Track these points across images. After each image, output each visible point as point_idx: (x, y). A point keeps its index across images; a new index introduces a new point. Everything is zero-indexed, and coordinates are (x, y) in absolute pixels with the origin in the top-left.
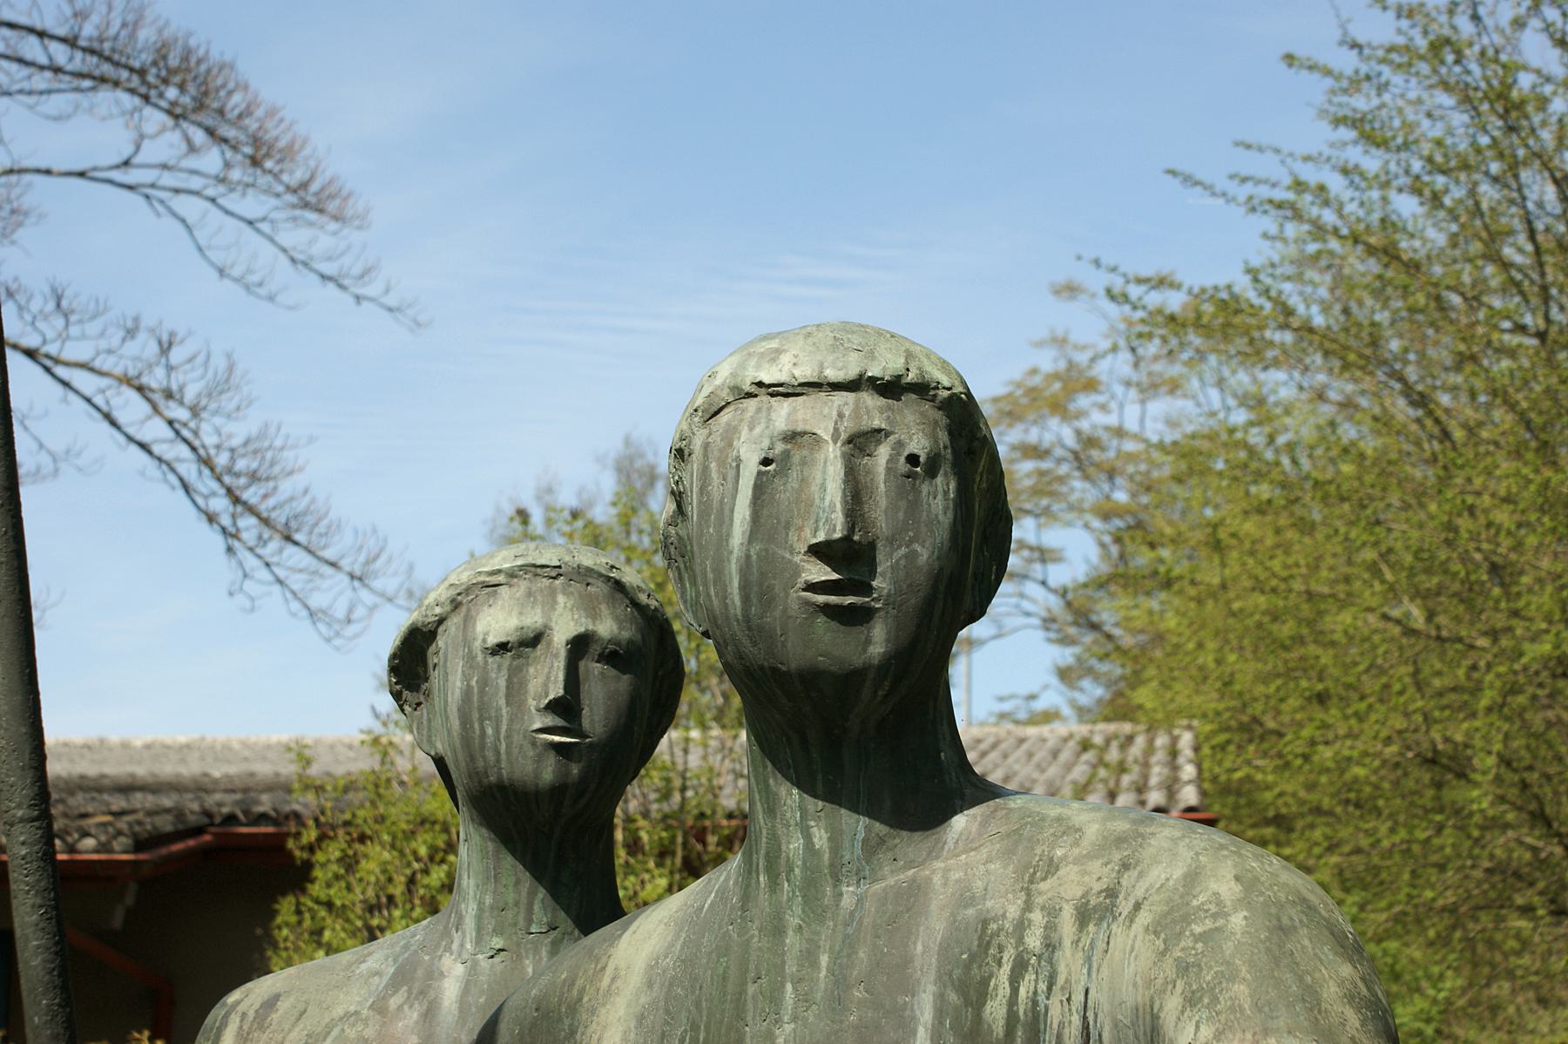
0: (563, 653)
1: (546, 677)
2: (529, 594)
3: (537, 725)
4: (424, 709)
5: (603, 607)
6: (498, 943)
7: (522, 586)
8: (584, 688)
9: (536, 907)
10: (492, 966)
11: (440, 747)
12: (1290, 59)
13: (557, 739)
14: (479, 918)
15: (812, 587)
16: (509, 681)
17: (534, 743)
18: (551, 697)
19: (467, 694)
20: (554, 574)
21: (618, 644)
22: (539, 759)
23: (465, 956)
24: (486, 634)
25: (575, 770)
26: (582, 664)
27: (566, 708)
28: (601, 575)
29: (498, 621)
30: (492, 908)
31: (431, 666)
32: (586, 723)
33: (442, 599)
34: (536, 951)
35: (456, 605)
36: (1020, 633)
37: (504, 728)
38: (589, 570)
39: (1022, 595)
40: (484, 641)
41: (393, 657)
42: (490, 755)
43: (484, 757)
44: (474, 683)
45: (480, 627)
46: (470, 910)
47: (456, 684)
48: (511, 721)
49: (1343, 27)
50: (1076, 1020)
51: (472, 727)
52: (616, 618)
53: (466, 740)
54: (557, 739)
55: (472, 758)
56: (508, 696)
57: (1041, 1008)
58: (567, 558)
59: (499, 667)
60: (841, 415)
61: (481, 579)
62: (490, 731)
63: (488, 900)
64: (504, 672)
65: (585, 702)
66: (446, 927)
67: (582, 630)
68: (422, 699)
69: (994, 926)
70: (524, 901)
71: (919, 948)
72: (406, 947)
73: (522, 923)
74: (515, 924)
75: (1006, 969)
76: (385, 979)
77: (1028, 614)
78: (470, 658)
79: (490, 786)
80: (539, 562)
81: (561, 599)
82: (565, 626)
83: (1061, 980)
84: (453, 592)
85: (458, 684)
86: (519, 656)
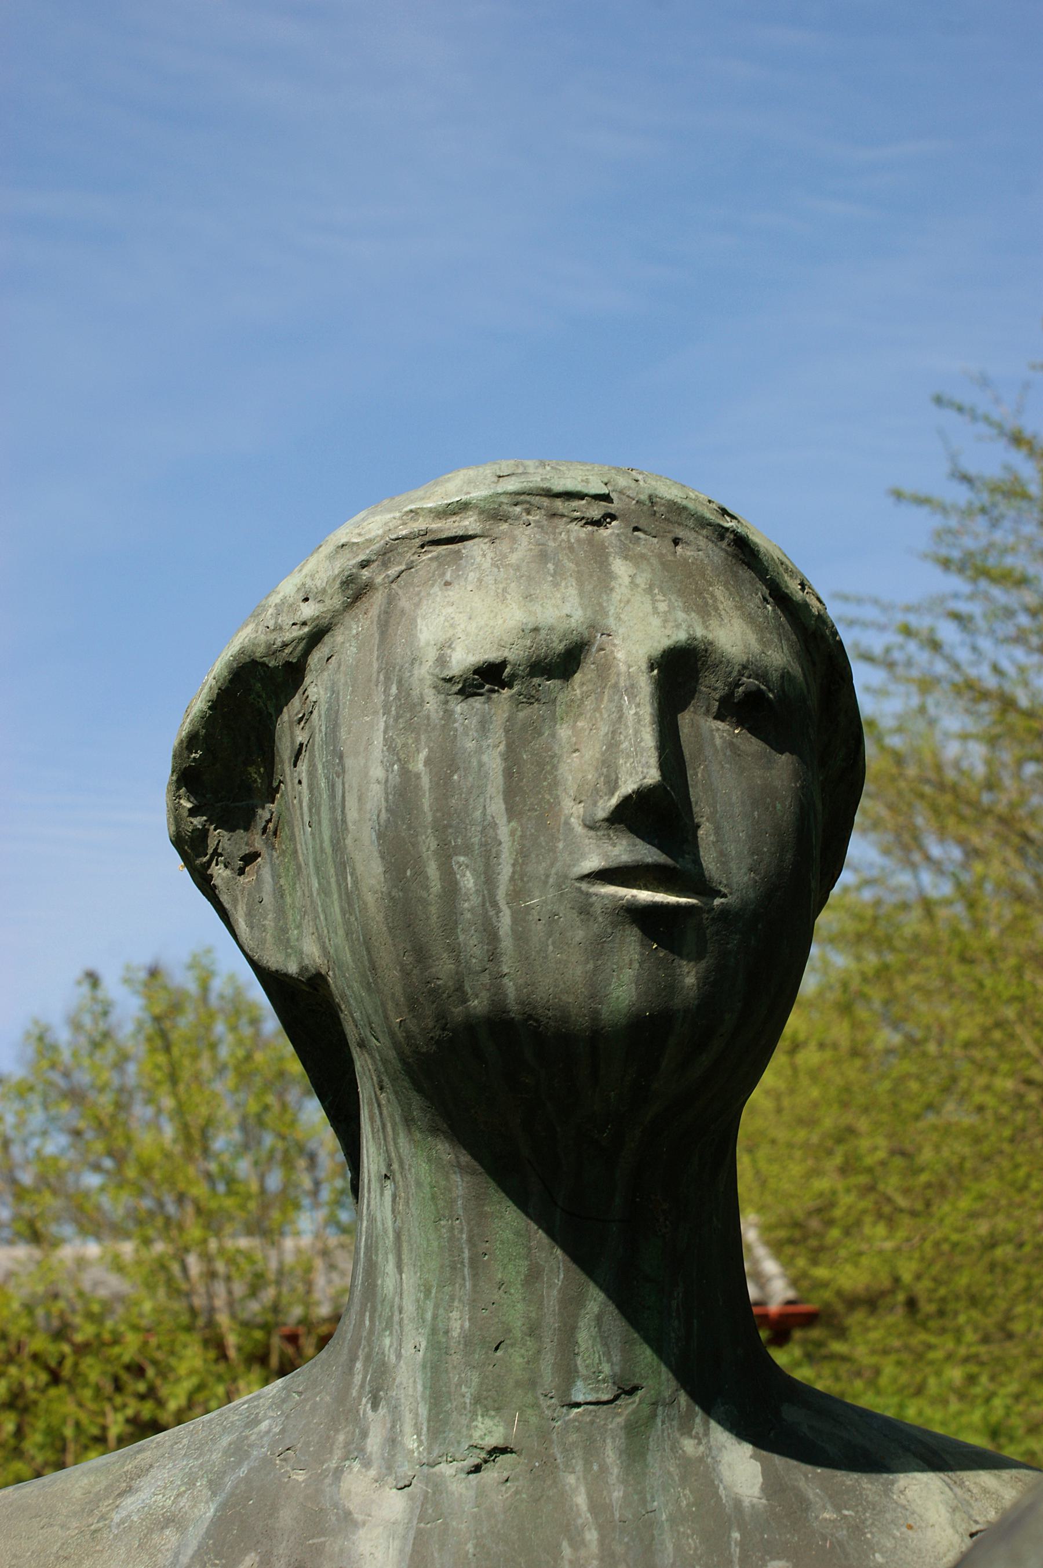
0: (645, 686)
1: (608, 743)
2: (543, 556)
3: (593, 863)
4: (263, 867)
5: (719, 591)
6: (489, 1431)
7: (523, 540)
8: (696, 775)
9: (584, 1336)
10: (481, 1493)
11: (306, 952)
12: (898, 495)
13: (644, 896)
14: (435, 1369)
16: (511, 757)
17: (585, 909)
18: (628, 787)
19: (402, 796)
20: (596, 511)
21: (762, 675)
22: (598, 948)
23: (406, 1470)
24: (445, 646)
25: (689, 976)
26: (685, 719)
27: (658, 815)
28: (703, 523)
29: (468, 617)
30: (468, 1342)
31: (284, 751)
32: (709, 860)
33: (320, 582)
34: (591, 1450)
35: (355, 590)
37: (505, 871)
38: (677, 511)
40: (442, 661)
41: (191, 741)
42: (471, 942)
43: (455, 951)
44: (419, 765)
45: (428, 630)
46: (407, 1353)
47: (369, 773)
48: (523, 855)
49: (953, 458)
51: (420, 873)
52: (750, 619)
53: (404, 909)
54: (644, 896)
55: (421, 954)
56: (511, 793)
58: (622, 482)
59: (484, 726)
61: (421, 524)
62: (468, 881)
63: (458, 1323)
64: (497, 735)
65: (702, 810)
66: (342, 1396)
67: (681, 636)
68: (258, 843)
70: (552, 1321)
72: (239, 1451)
73: (548, 1377)
74: (532, 1384)
76: (195, 1536)
78: (405, 709)
79: (471, 1026)
80: (560, 485)
81: (620, 568)
82: (640, 628)
84: (349, 561)
85: (377, 772)
86: (531, 699)
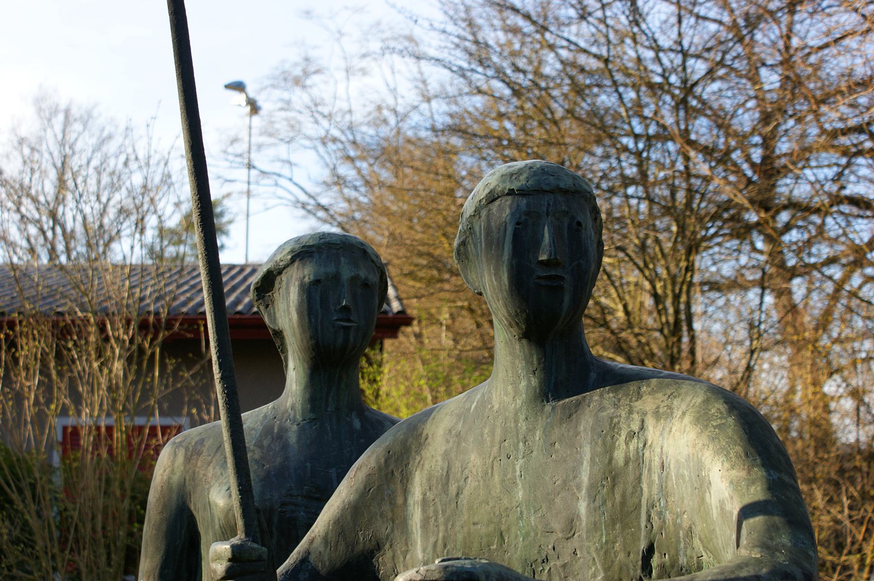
3: (335, 318)
9: (330, 400)
15: (539, 277)
36: (215, 191)
39: (276, 184)
50: (657, 459)
57: (641, 454)
60: (549, 205)
69: (616, 420)
71: (582, 428)
75: (623, 437)
77: (281, 198)
83: (649, 443)
